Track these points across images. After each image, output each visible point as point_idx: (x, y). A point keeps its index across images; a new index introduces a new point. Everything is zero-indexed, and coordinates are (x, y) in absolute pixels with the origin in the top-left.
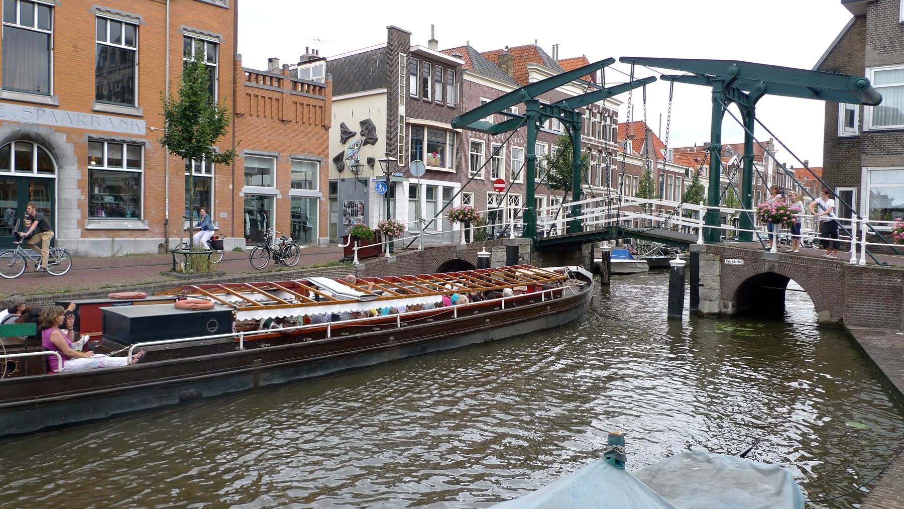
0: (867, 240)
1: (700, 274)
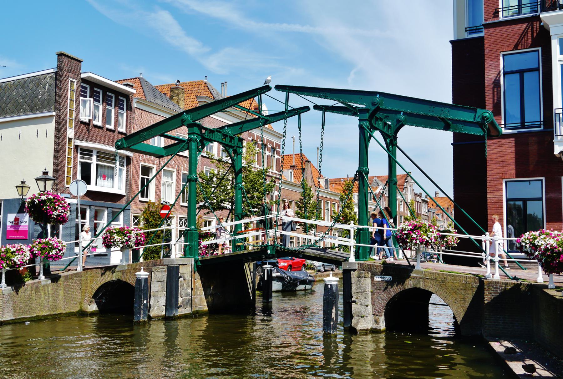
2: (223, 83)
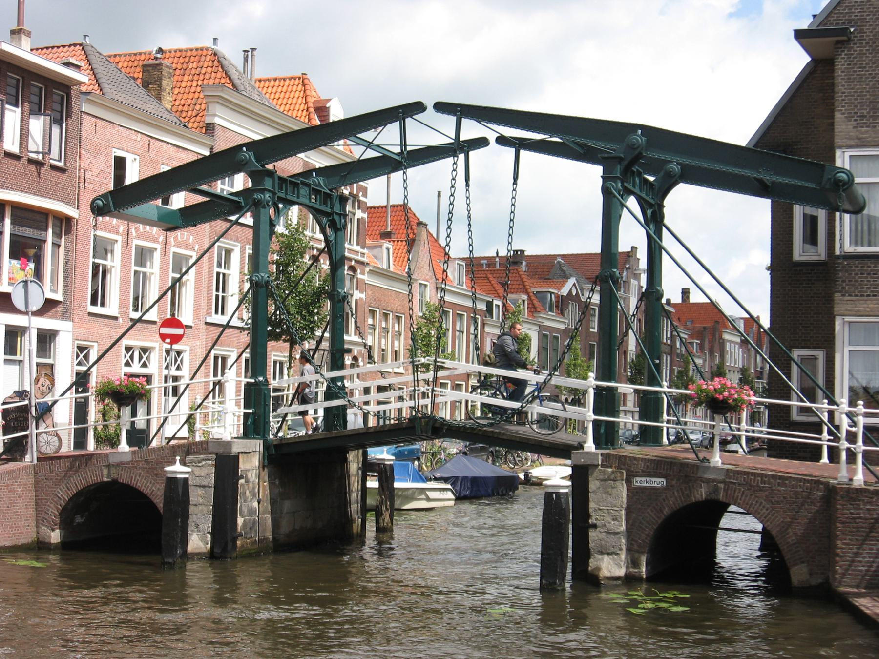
1: (592, 505)
2: (248, 51)
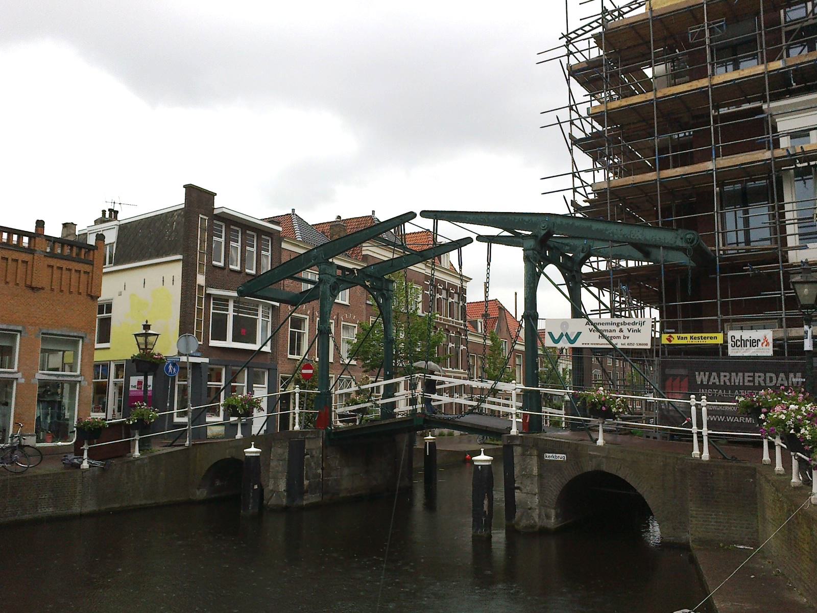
0: (709, 429)
